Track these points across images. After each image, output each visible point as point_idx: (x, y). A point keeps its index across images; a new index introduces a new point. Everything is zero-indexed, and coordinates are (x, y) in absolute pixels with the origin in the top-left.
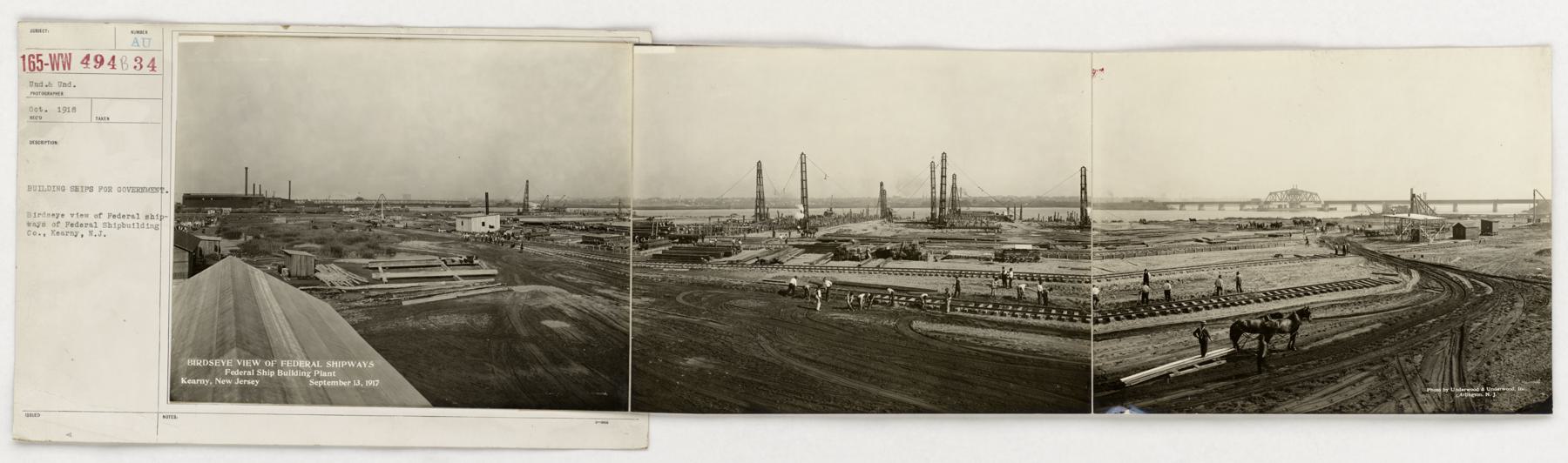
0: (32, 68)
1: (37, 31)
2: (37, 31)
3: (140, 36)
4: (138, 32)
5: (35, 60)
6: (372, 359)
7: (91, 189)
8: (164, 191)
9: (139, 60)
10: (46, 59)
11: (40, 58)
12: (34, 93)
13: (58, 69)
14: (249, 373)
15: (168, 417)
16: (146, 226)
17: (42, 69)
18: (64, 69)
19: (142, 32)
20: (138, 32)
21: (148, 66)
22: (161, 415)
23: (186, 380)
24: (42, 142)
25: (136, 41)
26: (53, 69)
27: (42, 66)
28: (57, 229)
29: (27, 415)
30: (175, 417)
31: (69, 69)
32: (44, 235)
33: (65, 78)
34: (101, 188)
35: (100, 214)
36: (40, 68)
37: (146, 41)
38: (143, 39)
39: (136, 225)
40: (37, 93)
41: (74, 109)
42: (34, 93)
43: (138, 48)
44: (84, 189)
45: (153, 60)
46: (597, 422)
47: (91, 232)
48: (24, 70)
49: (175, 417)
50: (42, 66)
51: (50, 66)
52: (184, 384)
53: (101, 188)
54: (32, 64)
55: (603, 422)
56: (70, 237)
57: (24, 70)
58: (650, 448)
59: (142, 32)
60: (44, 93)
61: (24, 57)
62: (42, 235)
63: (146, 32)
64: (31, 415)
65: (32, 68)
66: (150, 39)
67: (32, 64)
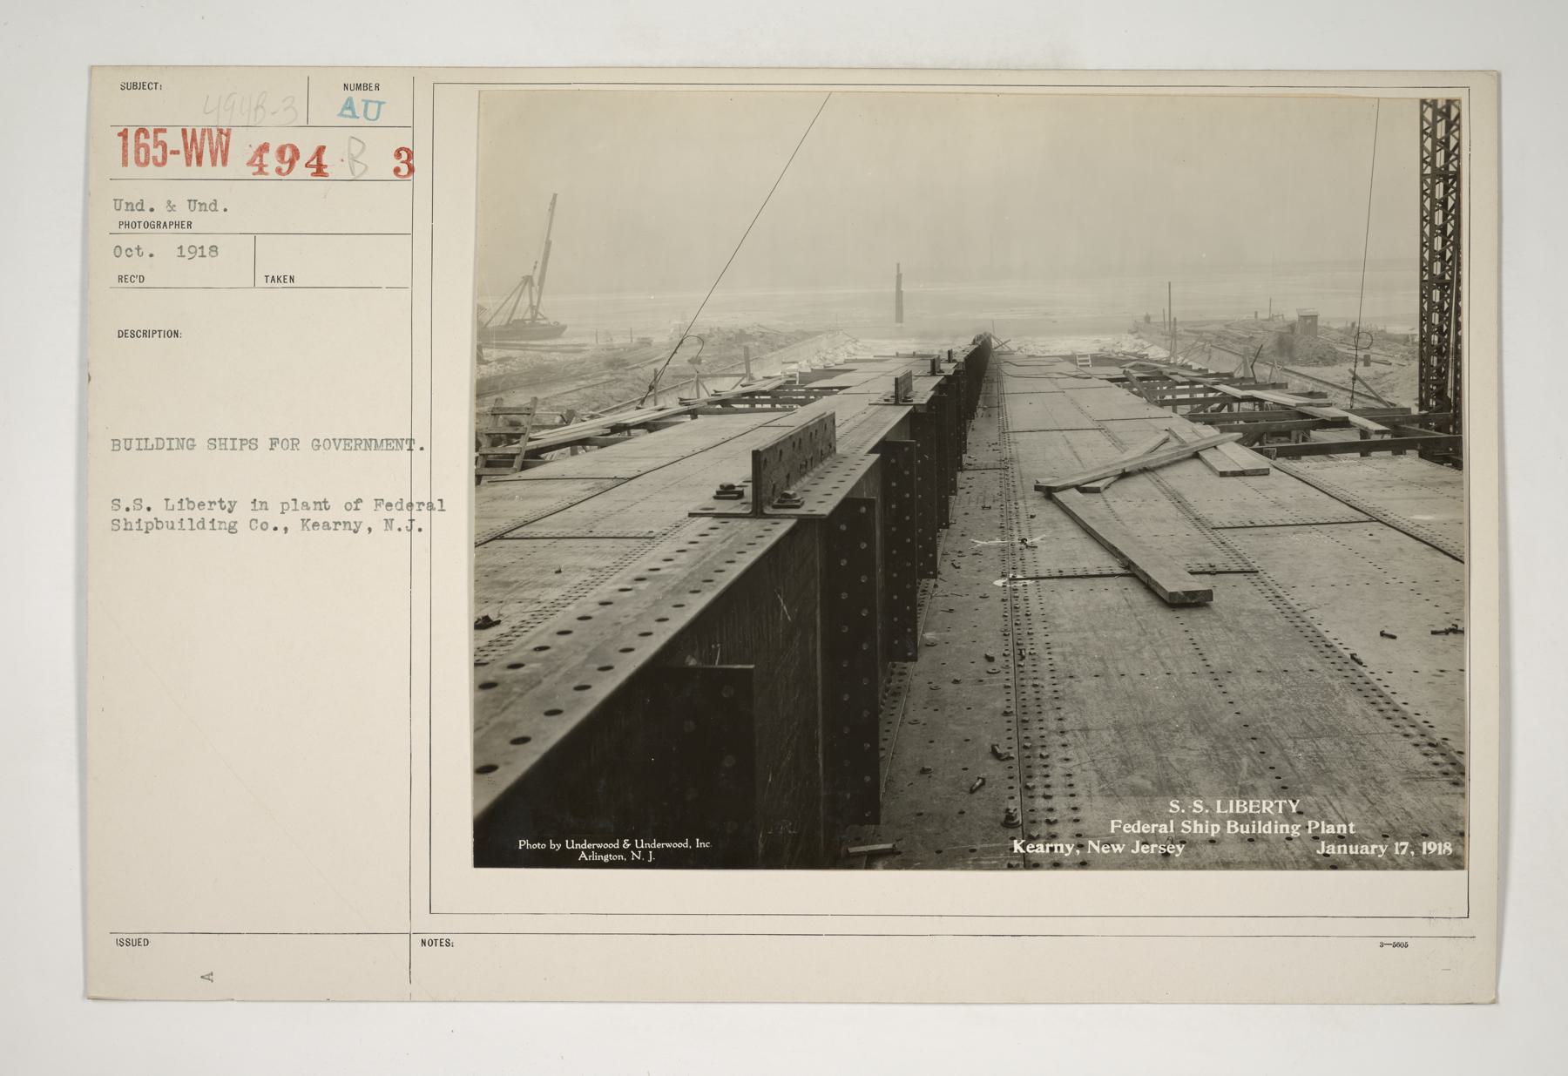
0: (142, 159)
1: (135, 86)
2: (135, 86)
3: (358, 96)
4: (359, 87)
5: (150, 142)
6: (1199, 797)
7: (317, 444)
8: (416, 447)
9: (288, 154)
10: (174, 140)
11: (161, 137)
12: (127, 225)
13: (199, 163)
14: (1163, 829)
15: (432, 943)
16: (207, 526)
17: (164, 163)
18: (214, 163)
19: (367, 87)
20: (359, 87)
21: (307, 165)
22: (416, 940)
23: (1024, 846)
24: (145, 334)
25: (349, 105)
26: (188, 164)
27: (165, 158)
28: (261, 516)
29: (121, 943)
30: (448, 944)
31: (224, 162)
32: (286, 529)
33: (204, 193)
34: (274, 442)
35: (359, 501)
36: (160, 160)
37: (373, 108)
38: (367, 102)
39: (187, 524)
40: (135, 225)
41: (214, 248)
42: (127, 225)
43: (354, 122)
44: (238, 443)
45: (321, 150)
46: (1382, 945)
47: (389, 522)
48: (125, 163)
49: (448, 944)
50: (165, 158)
51: (182, 157)
52: (1229, 834)
53: (274, 442)
54: (142, 151)
55: (1395, 945)
56: (344, 535)
57: (125, 163)
58: (1501, 999)
59: (367, 87)
60: (148, 225)
61: (124, 134)
62: (281, 530)
63: (377, 87)
64: (128, 942)
65: (142, 159)
66: (380, 103)
67: (142, 151)
